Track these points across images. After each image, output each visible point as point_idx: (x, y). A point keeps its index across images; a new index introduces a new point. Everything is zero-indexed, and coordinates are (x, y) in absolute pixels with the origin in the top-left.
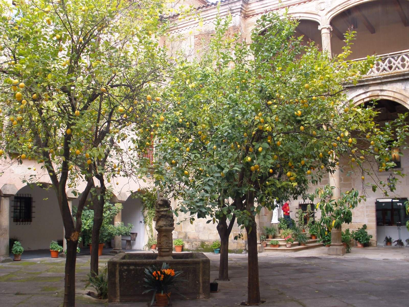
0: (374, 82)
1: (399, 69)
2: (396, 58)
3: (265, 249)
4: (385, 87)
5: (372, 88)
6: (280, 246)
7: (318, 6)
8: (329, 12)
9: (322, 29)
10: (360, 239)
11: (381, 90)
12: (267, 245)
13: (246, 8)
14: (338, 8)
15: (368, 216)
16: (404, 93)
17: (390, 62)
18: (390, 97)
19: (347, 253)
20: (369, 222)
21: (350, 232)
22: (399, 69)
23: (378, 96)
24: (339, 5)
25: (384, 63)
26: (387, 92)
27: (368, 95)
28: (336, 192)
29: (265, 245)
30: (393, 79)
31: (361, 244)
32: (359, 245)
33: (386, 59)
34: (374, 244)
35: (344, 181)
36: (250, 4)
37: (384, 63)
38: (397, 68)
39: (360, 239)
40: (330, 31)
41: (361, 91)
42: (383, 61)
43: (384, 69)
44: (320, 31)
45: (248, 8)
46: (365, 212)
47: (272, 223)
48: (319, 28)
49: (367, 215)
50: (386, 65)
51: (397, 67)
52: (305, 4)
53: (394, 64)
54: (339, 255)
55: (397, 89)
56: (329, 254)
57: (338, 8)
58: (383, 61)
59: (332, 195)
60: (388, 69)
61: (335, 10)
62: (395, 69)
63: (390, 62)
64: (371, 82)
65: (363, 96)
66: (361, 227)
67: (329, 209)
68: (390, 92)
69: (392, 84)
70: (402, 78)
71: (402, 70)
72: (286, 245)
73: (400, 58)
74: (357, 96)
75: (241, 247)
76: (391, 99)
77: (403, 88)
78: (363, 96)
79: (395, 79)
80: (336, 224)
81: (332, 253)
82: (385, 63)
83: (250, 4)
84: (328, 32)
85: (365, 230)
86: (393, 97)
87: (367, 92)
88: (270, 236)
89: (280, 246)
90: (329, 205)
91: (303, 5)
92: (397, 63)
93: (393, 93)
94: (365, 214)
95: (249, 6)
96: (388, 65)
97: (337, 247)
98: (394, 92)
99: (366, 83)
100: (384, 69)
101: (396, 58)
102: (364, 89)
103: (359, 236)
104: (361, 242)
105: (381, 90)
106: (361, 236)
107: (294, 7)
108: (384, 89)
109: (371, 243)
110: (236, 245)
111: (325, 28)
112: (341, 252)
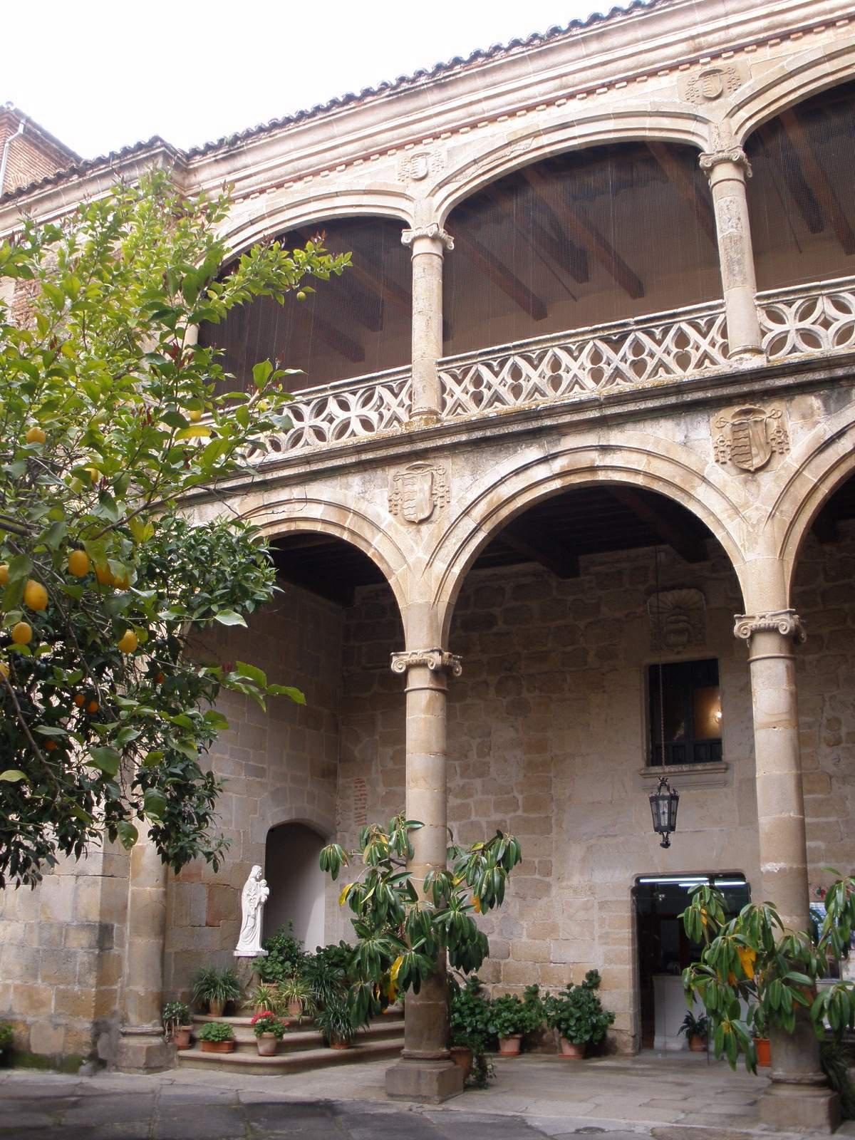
0: (576, 417)
1: (668, 371)
2: (658, 332)
3: (182, 1058)
4: (615, 437)
5: (570, 442)
6: (235, 1046)
7: (409, 166)
8: (441, 186)
9: (415, 239)
10: (569, 1027)
11: (605, 449)
12: (192, 1042)
13: (181, 186)
14: (473, 171)
15: (605, 938)
16: (682, 457)
17: (638, 348)
18: (637, 472)
19: (467, 1087)
20: (609, 960)
21: (542, 994)
22: (668, 371)
23: (593, 469)
24: (475, 162)
25: (616, 351)
26: (625, 454)
27: (558, 465)
28: (424, 843)
29: (182, 1039)
30: (642, 406)
31: (572, 1045)
32: (569, 1051)
33: (624, 337)
34: (625, 1044)
35: (525, 811)
36: (196, 170)
37: (616, 351)
38: (661, 370)
39: (569, 1027)
40: (445, 250)
41: (532, 453)
42: (616, 345)
43: (618, 373)
44: (408, 249)
45: (191, 186)
46: (596, 925)
47: (236, 954)
48: (406, 238)
49: (600, 937)
50: (624, 359)
51: (661, 364)
52: (369, 163)
53: (652, 355)
54: (425, 1099)
55: (658, 441)
56: (391, 1096)
57: (473, 171)
58: (616, 345)
59: (410, 855)
60: (630, 373)
61: (462, 180)
62: (655, 372)
63: (638, 348)
64: (567, 419)
65: (541, 472)
66: (580, 980)
67: (383, 911)
68: (635, 456)
69: (640, 426)
70: (672, 400)
71: (679, 375)
72: (254, 1045)
73: (672, 332)
74: (517, 472)
75: (79, 1044)
76: (639, 481)
77: (680, 438)
78: (541, 472)
79: (650, 404)
80: (407, 969)
81: (400, 1089)
82: (621, 353)
83: (196, 170)
84: (437, 249)
85: (596, 993)
86: (646, 474)
87: (555, 456)
88: (216, 1005)
89: (235, 1046)
90: (385, 894)
91: (361, 169)
92: (661, 351)
93: (644, 458)
94: (597, 931)
95: (193, 179)
96: (631, 358)
97: (423, 1066)
98: (649, 453)
99: (548, 422)
100: (618, 373)
101: (658, 332)
102: (542, 446)
103: (566, 1014)
104: (571, 1038)
105: (605, 449)
106: (571, 1015)
107: (333, 174)
108: (612, 443)
109: (613, 1041)
110: (62, 1040)
111: (425, 237)
112: (435, 1086)
